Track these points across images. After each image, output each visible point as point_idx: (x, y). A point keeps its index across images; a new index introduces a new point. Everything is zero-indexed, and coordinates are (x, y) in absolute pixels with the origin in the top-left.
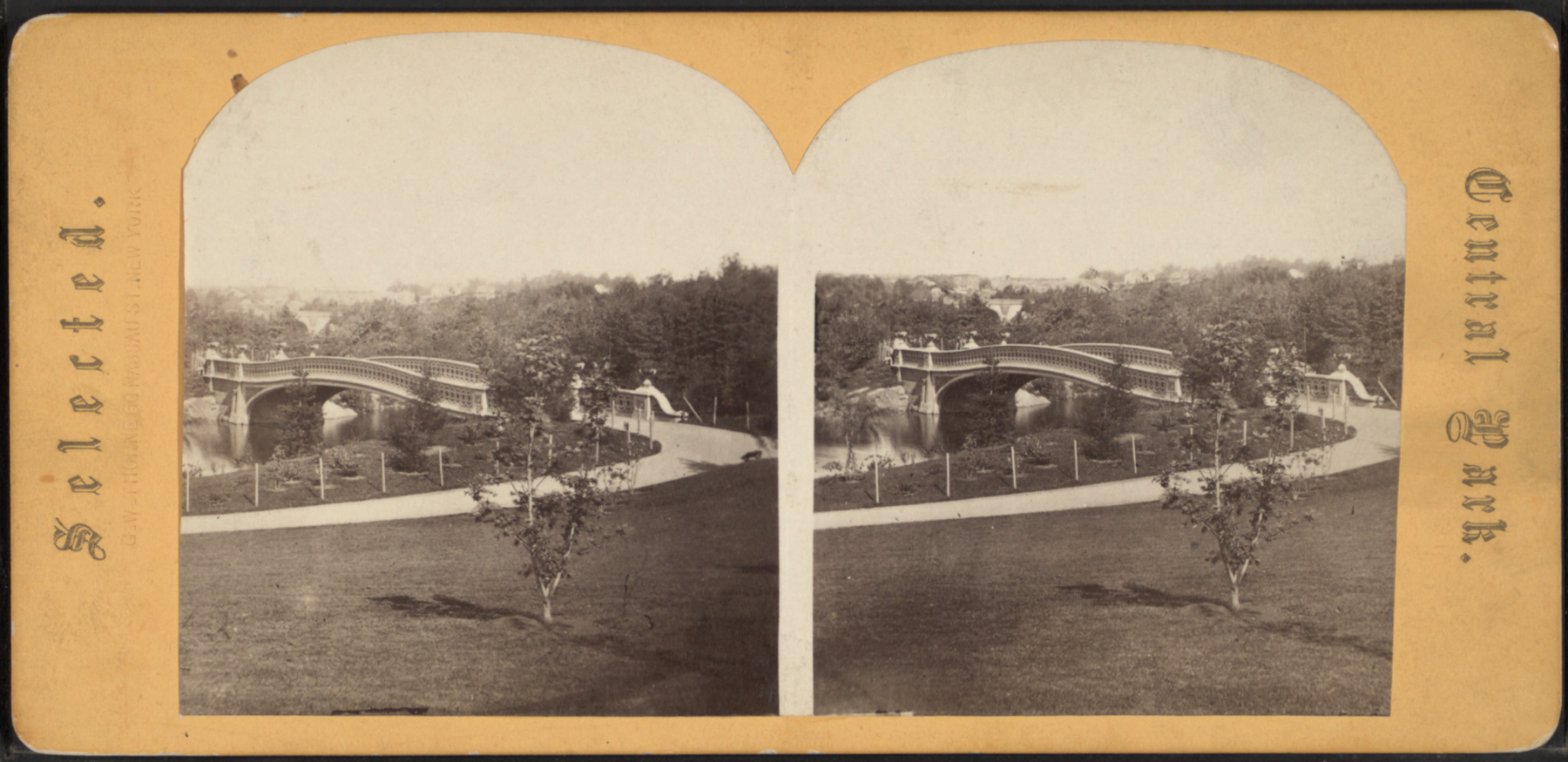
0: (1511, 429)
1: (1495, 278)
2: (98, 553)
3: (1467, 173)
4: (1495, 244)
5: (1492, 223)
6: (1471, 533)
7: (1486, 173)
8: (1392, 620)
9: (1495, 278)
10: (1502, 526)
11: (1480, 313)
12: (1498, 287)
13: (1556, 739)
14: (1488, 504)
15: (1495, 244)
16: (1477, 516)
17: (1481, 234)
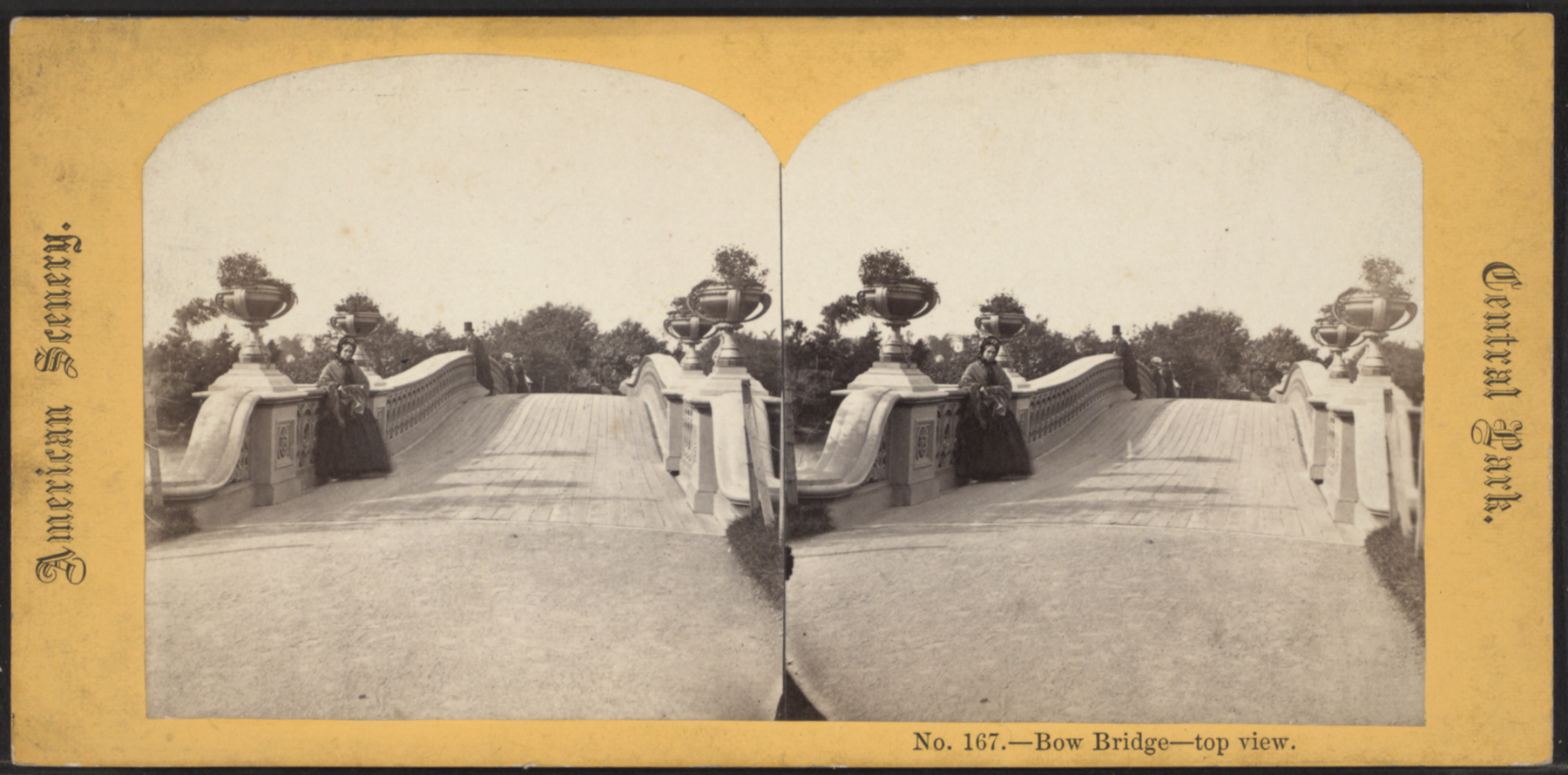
0: (1524, 436)
2: (71, 372)
3: (1490, 260)
4: (68, 279)
8: (404, 369)
9: (1509, 340)
10: (1518, 498)
11: (1497, 364)
12: (1511, 347)
14: (1505, 482)
15: (68, 279)
16: (1497, 490)
17: (1496, 309)
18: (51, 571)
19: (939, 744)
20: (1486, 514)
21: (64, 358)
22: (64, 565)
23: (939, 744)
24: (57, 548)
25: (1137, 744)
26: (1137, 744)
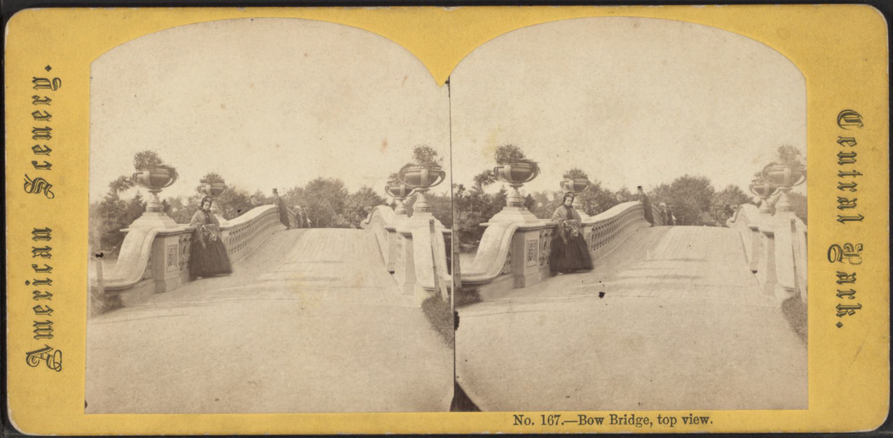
1: (855, 174)
5: (853, 141)
6: (842, 310)
7: (850, 114)
10: (859, 307)
11: (847, 194)
13: (887, 425)
14: (852, 294)
16: (846, 301)
18: (37, 359)
19: (528, 421)
20: (838, 319)
21: (44, 186)
22: (45, 356)
23: (528, 421)
24: (41, 343)
25: (631, 421)
26: (631, 421)
